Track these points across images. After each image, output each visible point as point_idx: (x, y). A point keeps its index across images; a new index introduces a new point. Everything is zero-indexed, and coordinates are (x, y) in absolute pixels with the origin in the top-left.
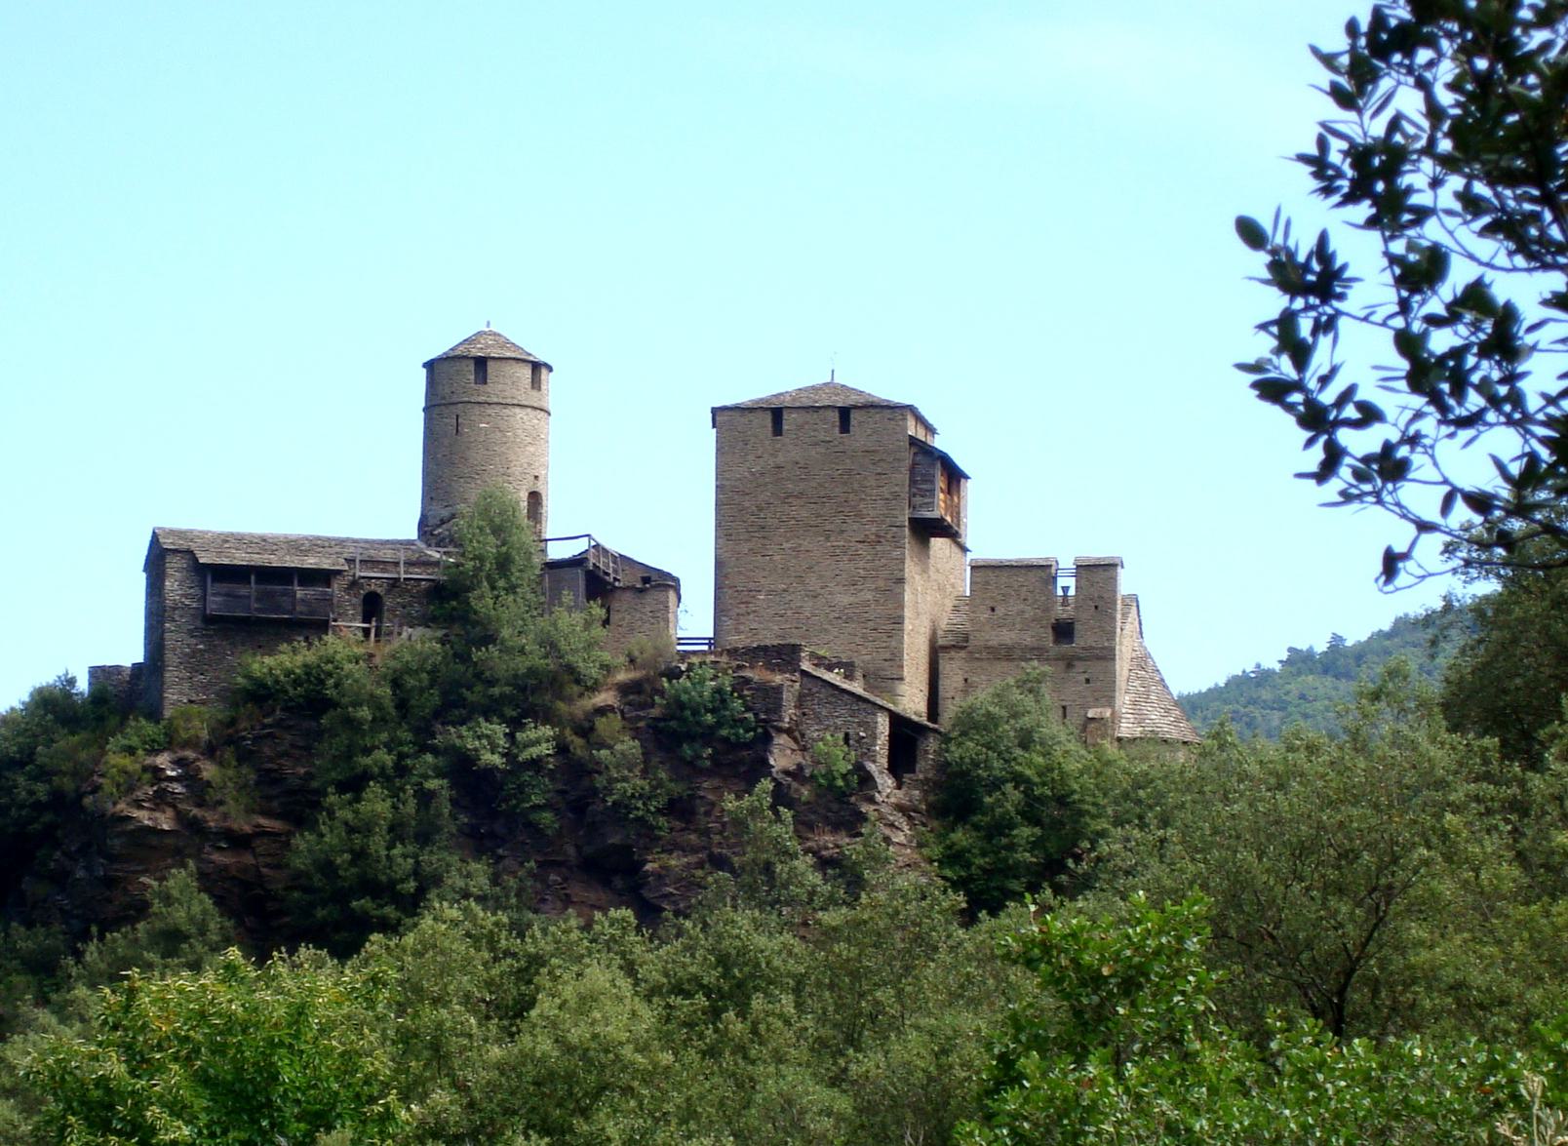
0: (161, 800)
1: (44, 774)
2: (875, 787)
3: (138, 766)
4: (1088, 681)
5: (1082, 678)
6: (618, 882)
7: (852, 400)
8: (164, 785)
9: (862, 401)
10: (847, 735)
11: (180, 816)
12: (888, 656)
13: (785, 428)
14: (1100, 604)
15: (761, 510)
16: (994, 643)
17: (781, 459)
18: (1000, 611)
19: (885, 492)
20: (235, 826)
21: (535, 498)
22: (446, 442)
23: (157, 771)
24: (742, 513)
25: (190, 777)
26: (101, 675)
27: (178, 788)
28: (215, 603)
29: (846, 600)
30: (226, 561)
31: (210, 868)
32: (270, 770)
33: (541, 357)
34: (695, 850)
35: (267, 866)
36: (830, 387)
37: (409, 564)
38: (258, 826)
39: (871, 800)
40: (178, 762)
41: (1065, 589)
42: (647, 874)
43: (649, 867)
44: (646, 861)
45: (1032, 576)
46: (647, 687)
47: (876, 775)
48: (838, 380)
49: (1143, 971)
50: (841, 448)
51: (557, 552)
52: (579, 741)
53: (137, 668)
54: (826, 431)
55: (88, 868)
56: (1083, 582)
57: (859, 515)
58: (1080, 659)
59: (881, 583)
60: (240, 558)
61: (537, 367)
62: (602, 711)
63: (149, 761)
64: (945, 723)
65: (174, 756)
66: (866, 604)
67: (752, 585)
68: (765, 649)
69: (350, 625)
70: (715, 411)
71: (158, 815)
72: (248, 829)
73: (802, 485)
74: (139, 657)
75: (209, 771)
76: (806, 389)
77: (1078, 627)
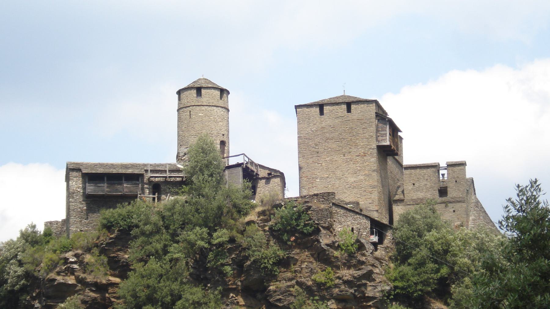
0: (72, 271)
1: (21, 264)
2: (365, 249)
3: (57, 258)
4: (454, 211)
5: (452, 210)
6: (259, 296)
7: (351, 100)
8: (69, 265)
9: (355, 100)
10: (353, 229)
11: (77, 279)
12: (371, 202)
13: (325, 112)
14: (458, 180)
15: (316, 145)
16: (415, 198)
17: (323, 125)
18: (417, 185)
19: (367, 135)
20: (99, 281)
21: (223, 143)
22: (186, 122)
23: (66, 259)
24: (307, 147)
25: (80, 262)
26: (49, 225)
27: (76, 266)
28: (91, 189)
29: (353, 180)
30: (94, 172)
31: (87, 299)
32: (114, 257)
33: (224, 87)
34: (290, 280)
35: (114, 297)
36: (343, 96)
37: (171, 171)
38: (109, 280)
39: (364, 255)
40: (76, 255)
41: (443, 175)
42: (270, 291)
43: (271, 288)
44: (269, 286)
45: (430, 170)
46: (268, 213)
47: (365, 244)
48: (347, 94)
49: (485, 251)
50: (348, 119)
51: (232, 161)
52: (240, 236)
53: (64, 221)
54: (342, 112)
55: (40, 303)
56: (450, 172)
57: (356, 145)
58: (450, 202)
59: (367, 172)
60: (100, 171)
61: (223, 92)
62: (249, 223)
63: (63, 256)
64: (395, 224)
65: (74, 253)
66: (361, 181)
67: (314, 176)
68: (316, 195)
69: (148, 196)
70: (297, 107)
71: (66, 278)
72: (104, 282)
73: (333, 135)
74: (64, 217)
75: (88, 258)
76: (333, 98)
77: (448, 189)
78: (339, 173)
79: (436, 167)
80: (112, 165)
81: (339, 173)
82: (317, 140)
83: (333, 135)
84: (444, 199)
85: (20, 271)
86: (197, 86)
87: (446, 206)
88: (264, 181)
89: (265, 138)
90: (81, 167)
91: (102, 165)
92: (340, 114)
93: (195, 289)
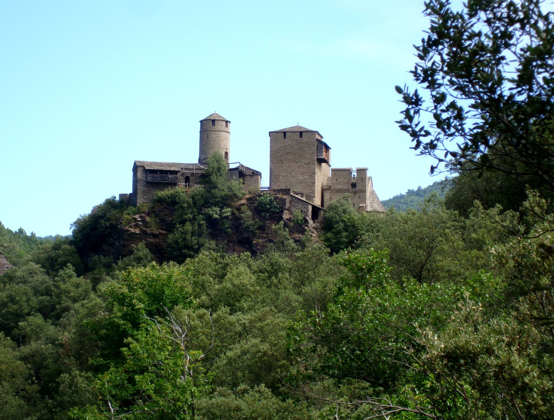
1: (108, 220)
2: (308, 223)
7: (303, 130)
9: (305, 130)
11: (141, 230)
17: (286, 144)
18: (339, 180)
23: (135, 219)
24: (276, 157)
25: (143, 221)
26: (121, 196)
27: (140, 223)
28: (149, 179)
29: (301, 178)
31: (148, 242)
33: (228, 120)
36: (298, 127)
37: (196, 169)
40: (141, 217)
42: (254, 244)
43: (254, 242)
45: (346, 172)
46: (253, 199)
51: (232, 166)
52: (237, 212)
60: (156, 168)
61: (227, 122)
62: (242, 205)
63: (133, 217)
66: (306, 179)
68: (282, 190)
70: (270, 133)
72: (157, 233)
75: (148, 219)
78: (293, 174)
79: (349, 171)
80: (161, 163)
81: (293, 174)
82: (281, 153)
83: (291, 151)
84: (354, 189)
85: (108, 224)
86: (212, 118)
87: (355, 194)
88: (249, 177)
89: (247, 149)
90: (144, 165)
91: (155, 164)
92: (295, 139)
93: (212, 242)
